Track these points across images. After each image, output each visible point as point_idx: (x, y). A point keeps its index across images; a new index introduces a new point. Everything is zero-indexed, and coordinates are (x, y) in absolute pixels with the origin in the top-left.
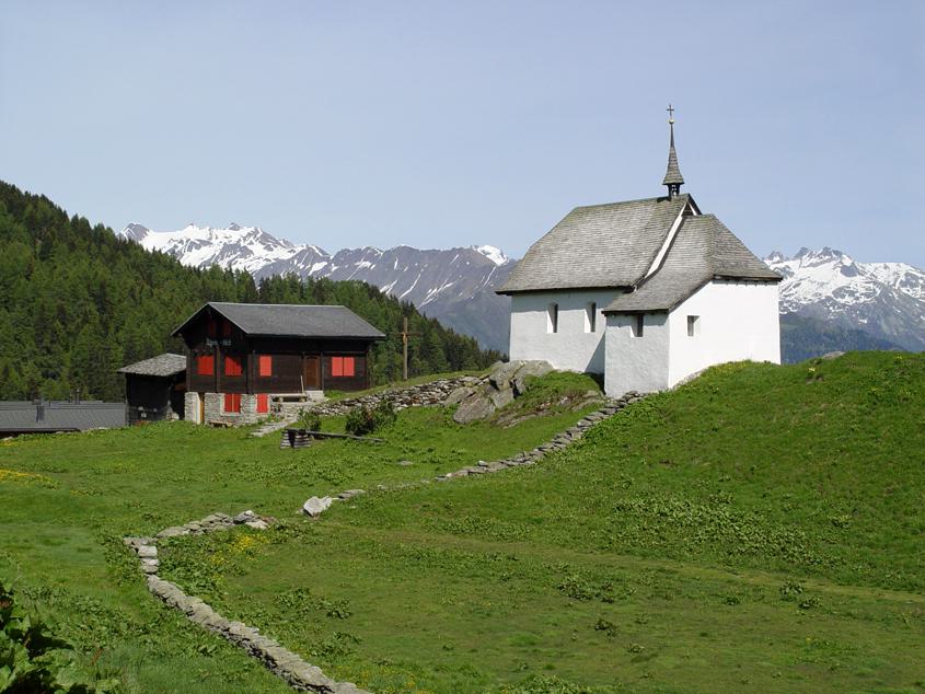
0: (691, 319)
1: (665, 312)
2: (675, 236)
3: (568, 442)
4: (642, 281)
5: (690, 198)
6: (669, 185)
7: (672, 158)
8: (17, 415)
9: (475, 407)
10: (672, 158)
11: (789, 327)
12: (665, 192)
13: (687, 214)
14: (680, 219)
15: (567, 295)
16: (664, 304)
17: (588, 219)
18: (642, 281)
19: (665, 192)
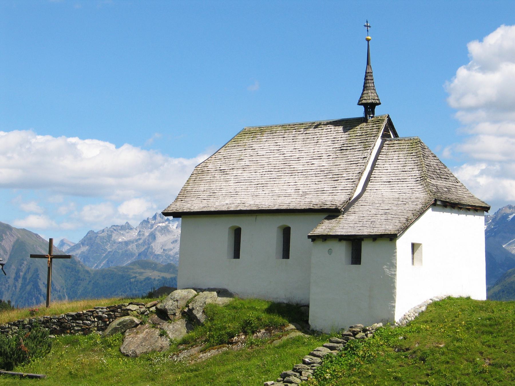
0: (414, 247)
1: (392, 238)
2: (376, 159)
3: (299, 381)
4: (350, 204)
5: (389, 120)
6: (365, 105)
7: (368, 78)
8: (3, 371)
9: (145, 339)
10: (368, 78)
11: (394, 269)
12: (360, 112)
13: (385, 136)
14: (379, 141)
15: (254, 218)
16: (390, 228)
17: (264, 139)
18: (350, 204)
19: (360, 112)
